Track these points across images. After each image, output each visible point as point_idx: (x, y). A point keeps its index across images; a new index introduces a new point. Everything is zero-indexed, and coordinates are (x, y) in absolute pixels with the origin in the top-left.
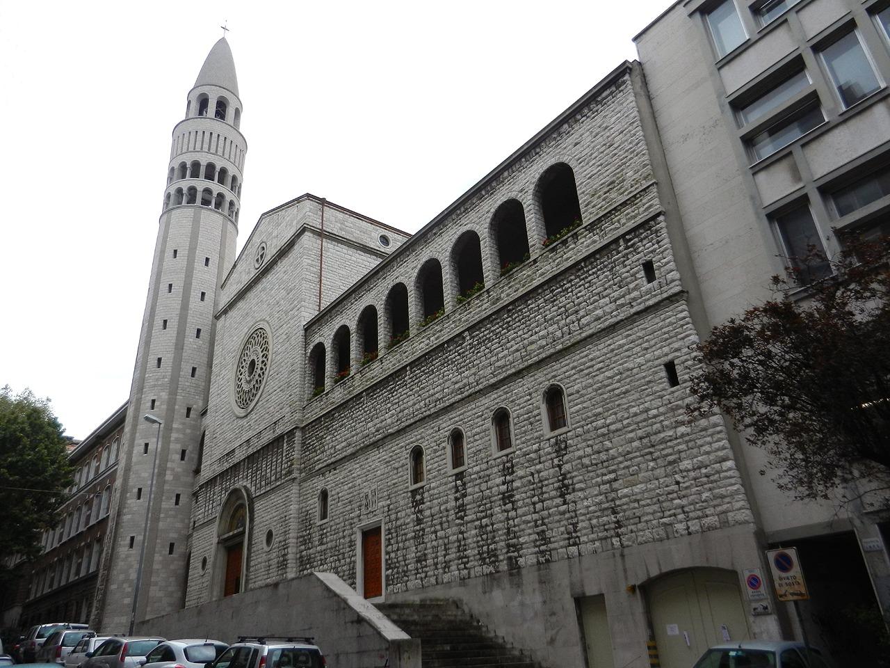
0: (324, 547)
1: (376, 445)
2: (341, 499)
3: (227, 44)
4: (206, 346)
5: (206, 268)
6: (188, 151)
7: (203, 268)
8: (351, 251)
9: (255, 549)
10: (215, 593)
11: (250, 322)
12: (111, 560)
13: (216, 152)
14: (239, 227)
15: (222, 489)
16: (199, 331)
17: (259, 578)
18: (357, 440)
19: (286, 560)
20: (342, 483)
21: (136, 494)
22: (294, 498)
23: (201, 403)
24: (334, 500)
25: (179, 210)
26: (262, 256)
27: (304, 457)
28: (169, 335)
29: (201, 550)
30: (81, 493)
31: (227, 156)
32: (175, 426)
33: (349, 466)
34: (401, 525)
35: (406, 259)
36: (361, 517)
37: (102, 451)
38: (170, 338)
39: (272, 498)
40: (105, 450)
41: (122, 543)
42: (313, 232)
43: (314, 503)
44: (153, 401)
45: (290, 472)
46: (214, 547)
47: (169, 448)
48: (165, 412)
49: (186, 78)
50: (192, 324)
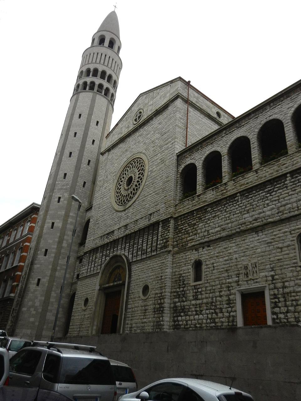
0: (198, 302)
1: (255, 230)
2: (215, 268)
3: (116, 13)
4: (92, 171)
5: (96, 127)
6: (92, 63)
7: (95, 126)
8: (202, 116)
9: (132, 297)
10: (95, 323)
11: (129, 155)
12: (24, 292)
13: (108, 65)
14: (114, 107)
15: (102, 255)
16: (89, 161)
17: (135, 317)
18: (233, 226)
19: (163, 308)
20: (217, 256)
21: (44, 252)
22: (169, 264)
23: (86, 203)
24: (209, 268)
25: (84, 93)
26: (139, 117)
27: (176, 237)
28: (72, 161)
29: (85, 293)
30: (4, 249)
31: (113, 69)
32: (71, 214)
33: (224, 244)
34: (290, 293)
35: (281, 103)
36: (240, 283)
37: (12, 231)
38: (73, 163)
39: (148, 263)
40: (14, 231)
41: (32, 282)
42: (183, 99)
43: (189, 271)
44: (59, 198)
45: (165, 247)
46: (96, 292)
47: (66, 227)
48: (66, 205)
49: (94, 27)
50: (87, 156)
